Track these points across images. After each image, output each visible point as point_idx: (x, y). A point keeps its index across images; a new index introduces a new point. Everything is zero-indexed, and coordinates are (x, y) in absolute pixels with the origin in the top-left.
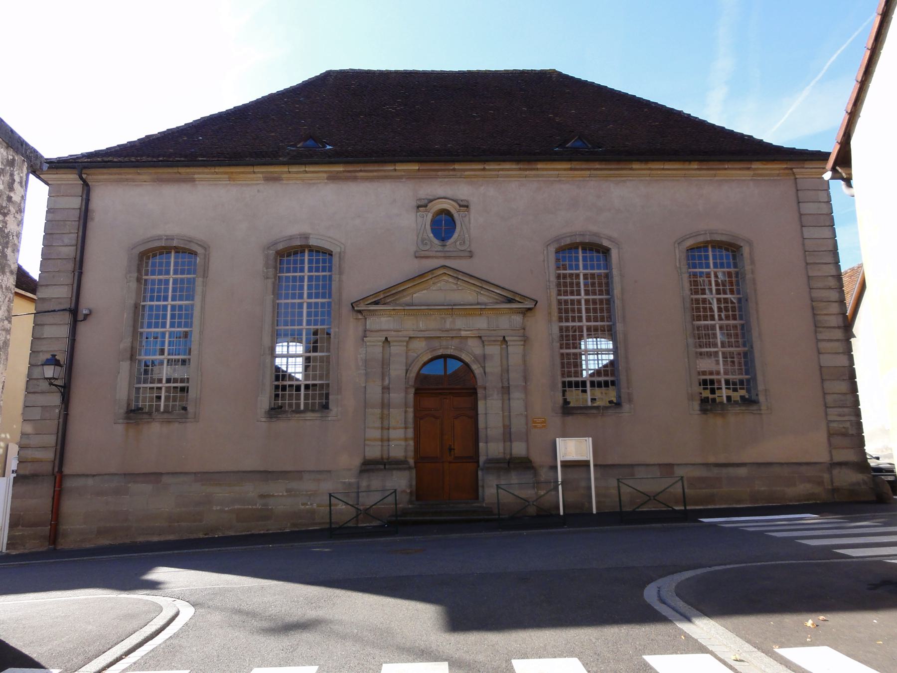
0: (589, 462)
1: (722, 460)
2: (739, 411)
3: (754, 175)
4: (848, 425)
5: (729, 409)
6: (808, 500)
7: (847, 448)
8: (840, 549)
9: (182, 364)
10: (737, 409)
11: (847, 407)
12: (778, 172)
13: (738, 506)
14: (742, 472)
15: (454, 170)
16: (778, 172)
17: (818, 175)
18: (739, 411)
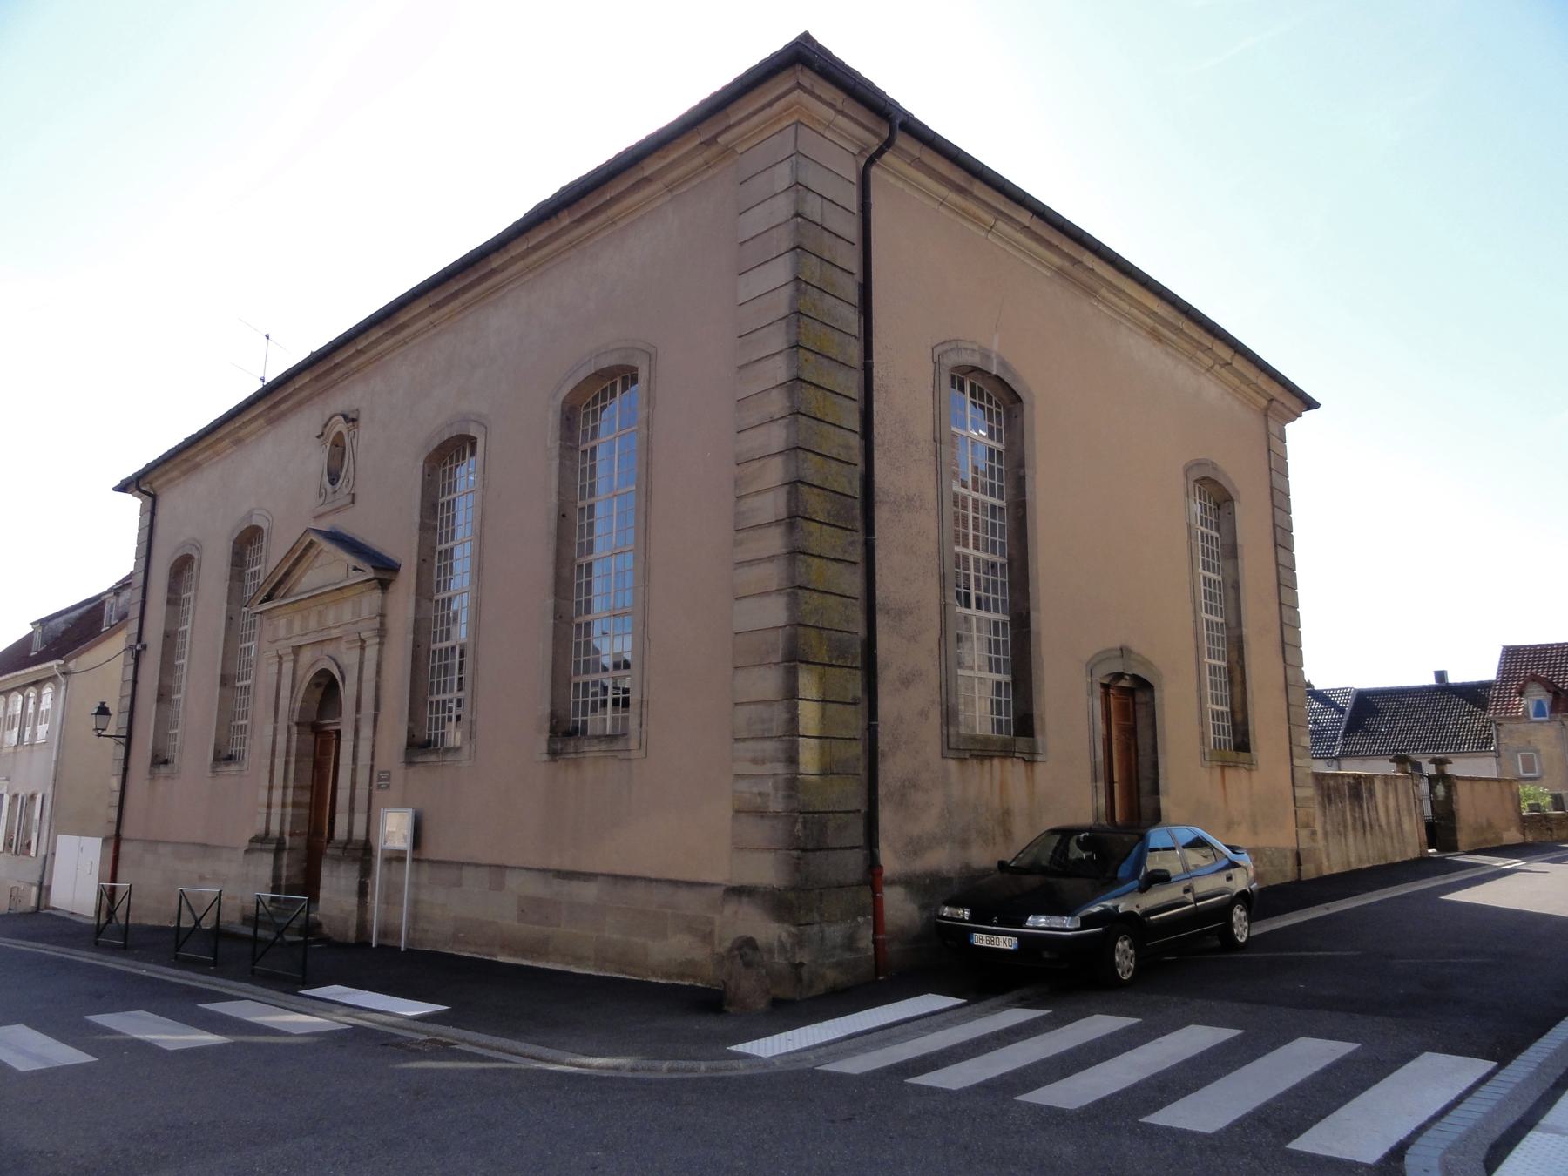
0: (405, 852)
1: (568, 866)
2: (597, 754)
3: (669, 188)
4: (768, 786)
5: (586, 749)
6: (682, 976)
7: (764, 850)
8: (848, 1053)
9: (597, 682)
10: (595, 749)
11: (770, 738)
12: (699, 160)
13: (577, 971)
14: (589, 892)
15: (337, 366)
16: (699, 160)
17: (775, 123)
18: (597, 754)
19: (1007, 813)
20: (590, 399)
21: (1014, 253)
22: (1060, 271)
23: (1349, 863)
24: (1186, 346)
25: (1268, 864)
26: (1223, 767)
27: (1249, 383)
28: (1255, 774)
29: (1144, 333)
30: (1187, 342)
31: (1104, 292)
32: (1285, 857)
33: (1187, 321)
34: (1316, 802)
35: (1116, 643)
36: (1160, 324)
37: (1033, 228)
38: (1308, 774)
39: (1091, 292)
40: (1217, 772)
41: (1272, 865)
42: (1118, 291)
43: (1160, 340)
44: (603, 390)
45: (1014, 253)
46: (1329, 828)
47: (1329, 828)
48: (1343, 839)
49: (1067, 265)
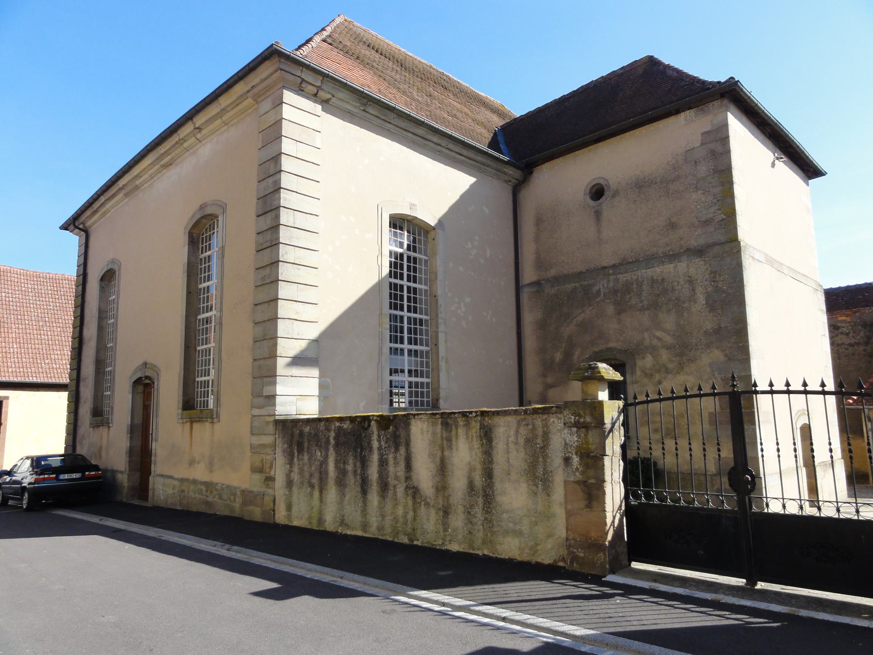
19: (101, 447)
20: (204, 230)
21: (149, 183)
22: (126, 195)
23: (320, 521)
24: (177, 151)
25: (217, 496)
26: (192, 423)
27: (224, 111)
28: (217, 426)
29: (164, 171)
30: (176, 149)
31: (138, 182)
32: (235, 495)
33: (160, 147)
34: (279, 451)
35: (141, 362)
36: (160, 162)
37: (107, 198)
38: (268, 423)
39: (137, 188)
40: (188, 425)
41: (220, 498)
42: (138, 176)
43: (171, 164)
44: (209, 225)
45: (149, 183)
46: (295, 476)
47: (295, 476)
48: (316, 494)
49: (124, 192)
